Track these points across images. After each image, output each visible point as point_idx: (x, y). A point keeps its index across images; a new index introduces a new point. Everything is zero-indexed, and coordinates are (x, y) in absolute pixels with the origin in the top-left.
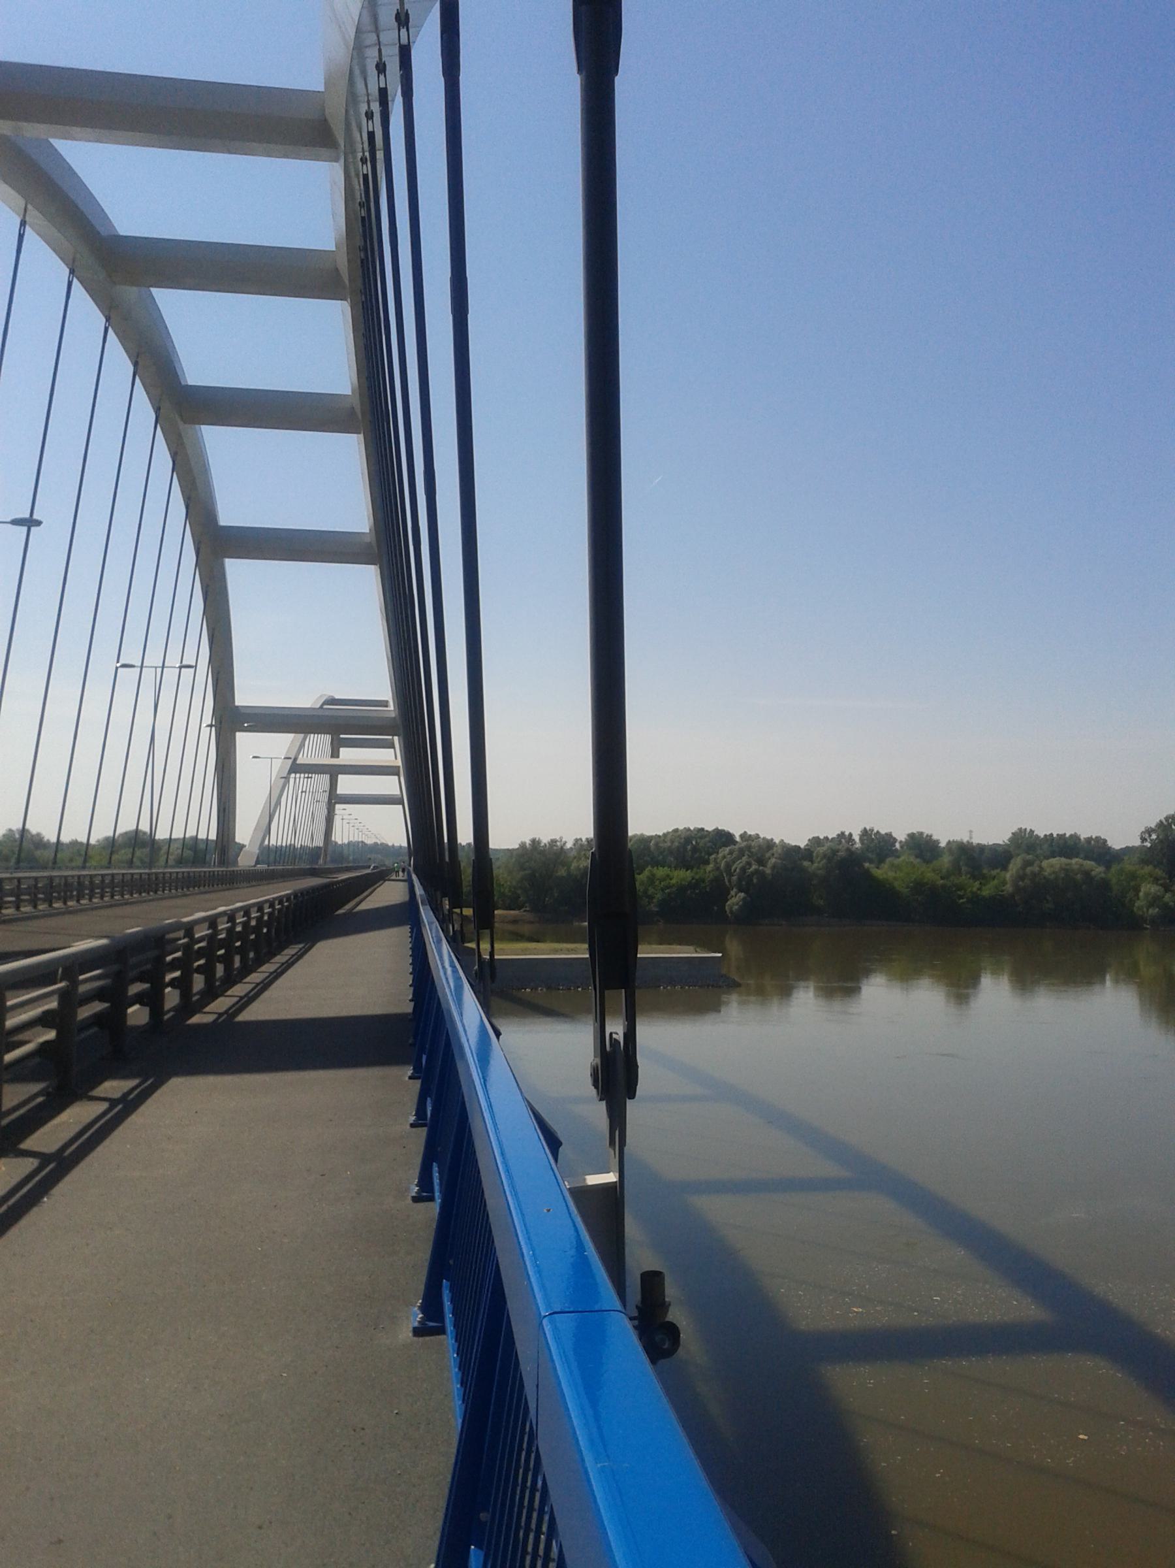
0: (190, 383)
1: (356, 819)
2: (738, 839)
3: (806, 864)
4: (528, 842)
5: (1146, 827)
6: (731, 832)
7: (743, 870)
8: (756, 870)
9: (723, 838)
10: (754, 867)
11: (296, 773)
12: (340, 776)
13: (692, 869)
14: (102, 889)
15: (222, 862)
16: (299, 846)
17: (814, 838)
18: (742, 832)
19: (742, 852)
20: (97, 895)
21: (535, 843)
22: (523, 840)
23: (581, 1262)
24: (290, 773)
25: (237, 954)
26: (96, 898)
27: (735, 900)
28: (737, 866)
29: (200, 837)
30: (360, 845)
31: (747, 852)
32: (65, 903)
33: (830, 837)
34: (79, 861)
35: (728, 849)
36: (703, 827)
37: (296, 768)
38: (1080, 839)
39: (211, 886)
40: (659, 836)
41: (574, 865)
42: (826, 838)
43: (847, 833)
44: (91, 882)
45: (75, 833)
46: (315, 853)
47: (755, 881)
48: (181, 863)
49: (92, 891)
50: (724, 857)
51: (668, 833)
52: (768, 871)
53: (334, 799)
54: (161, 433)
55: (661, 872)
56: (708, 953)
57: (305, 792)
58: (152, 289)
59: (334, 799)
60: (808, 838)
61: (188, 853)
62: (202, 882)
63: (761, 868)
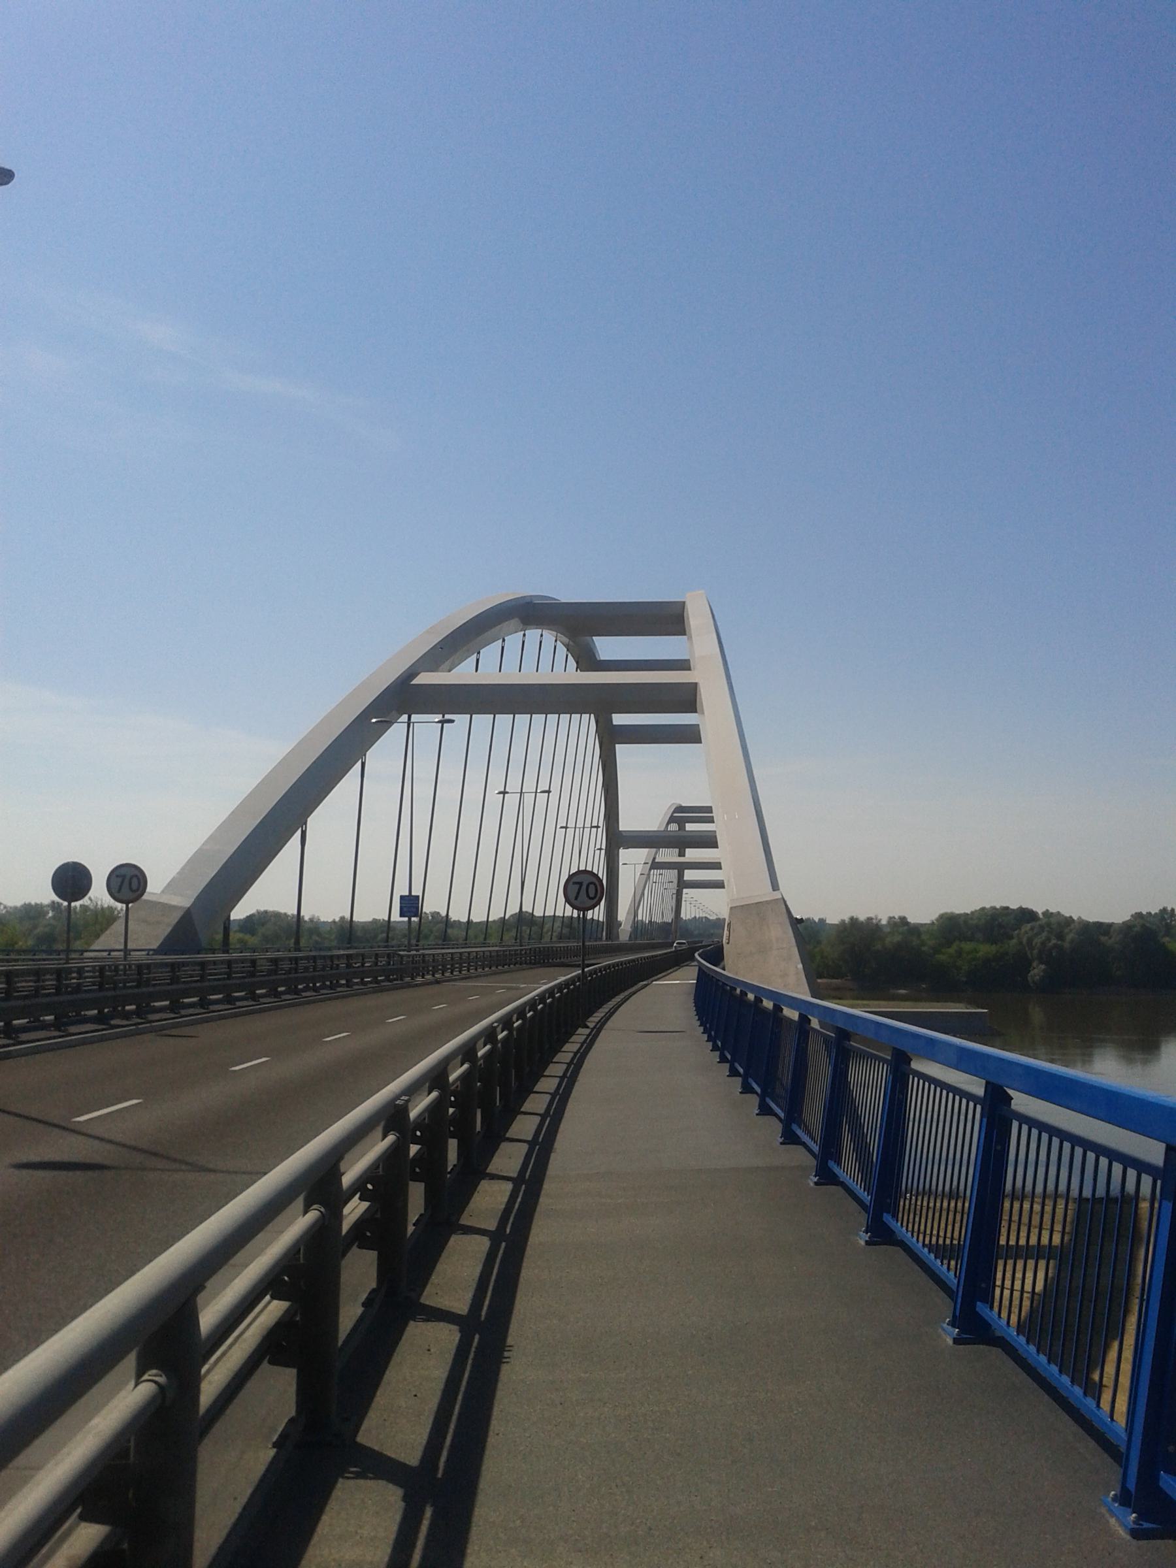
0: (602, 658)
1: (692, 898)
2: (1041, 916)
3: (1103, 939)
4: (847, 920)
5: (890, 918)
6: (1034, 910)
7: (1043, 943)
8: (1054, 944)
9: (1026, 915)
10: (1054, 941)
11: (654, 869)
12: (686, 871)
13: (996, 943)
14: (461, 964)
15: (609, 938)
16: (647, 922)
17: (1136, 913)
18: (1044, 910)
19: (1042, 928)
20: (457, 970)
21: (854, 921)
22: (843, 918)
23: (559, 600)
24: (650, 870)
25: (479, 1108)
26: (456, 971)
27: (1037, 971)
28: (1037, 941)
29: (536, 914)
30: (704, 920)
31: (1047, 929)
32: (433, 975)
33: (1153, 913)
34: (481, 939)
35: (1029, 926)
36: (984, 906)
37: (655, 865)
38: (815, 922)
39: (566, 958)
40: (967, 914)
41: (888, 940)
42: (1149, 914)
43: (1169, 909)
44: (452, 959)
45: (478, 917)
46: (665, 928)
47: (1054, 954)
48: (561, 938)
49: (469, 965)
50: (1026, 932)
51: (976, 911)
52: (1067, 945)
53: (682, 884)
54: (572, 658)
55: (967, 946)
56: (975, 1009)
57: (653, 882)
58: (594, 638)
59: (682, 884)
60: (1131, 914)
61: (566, 931)
62: (559, 955)
63: (1059, 942)
